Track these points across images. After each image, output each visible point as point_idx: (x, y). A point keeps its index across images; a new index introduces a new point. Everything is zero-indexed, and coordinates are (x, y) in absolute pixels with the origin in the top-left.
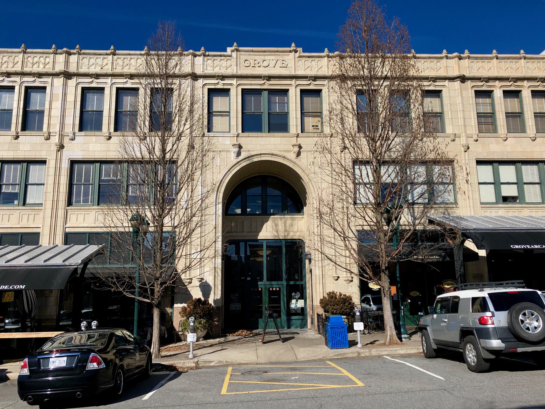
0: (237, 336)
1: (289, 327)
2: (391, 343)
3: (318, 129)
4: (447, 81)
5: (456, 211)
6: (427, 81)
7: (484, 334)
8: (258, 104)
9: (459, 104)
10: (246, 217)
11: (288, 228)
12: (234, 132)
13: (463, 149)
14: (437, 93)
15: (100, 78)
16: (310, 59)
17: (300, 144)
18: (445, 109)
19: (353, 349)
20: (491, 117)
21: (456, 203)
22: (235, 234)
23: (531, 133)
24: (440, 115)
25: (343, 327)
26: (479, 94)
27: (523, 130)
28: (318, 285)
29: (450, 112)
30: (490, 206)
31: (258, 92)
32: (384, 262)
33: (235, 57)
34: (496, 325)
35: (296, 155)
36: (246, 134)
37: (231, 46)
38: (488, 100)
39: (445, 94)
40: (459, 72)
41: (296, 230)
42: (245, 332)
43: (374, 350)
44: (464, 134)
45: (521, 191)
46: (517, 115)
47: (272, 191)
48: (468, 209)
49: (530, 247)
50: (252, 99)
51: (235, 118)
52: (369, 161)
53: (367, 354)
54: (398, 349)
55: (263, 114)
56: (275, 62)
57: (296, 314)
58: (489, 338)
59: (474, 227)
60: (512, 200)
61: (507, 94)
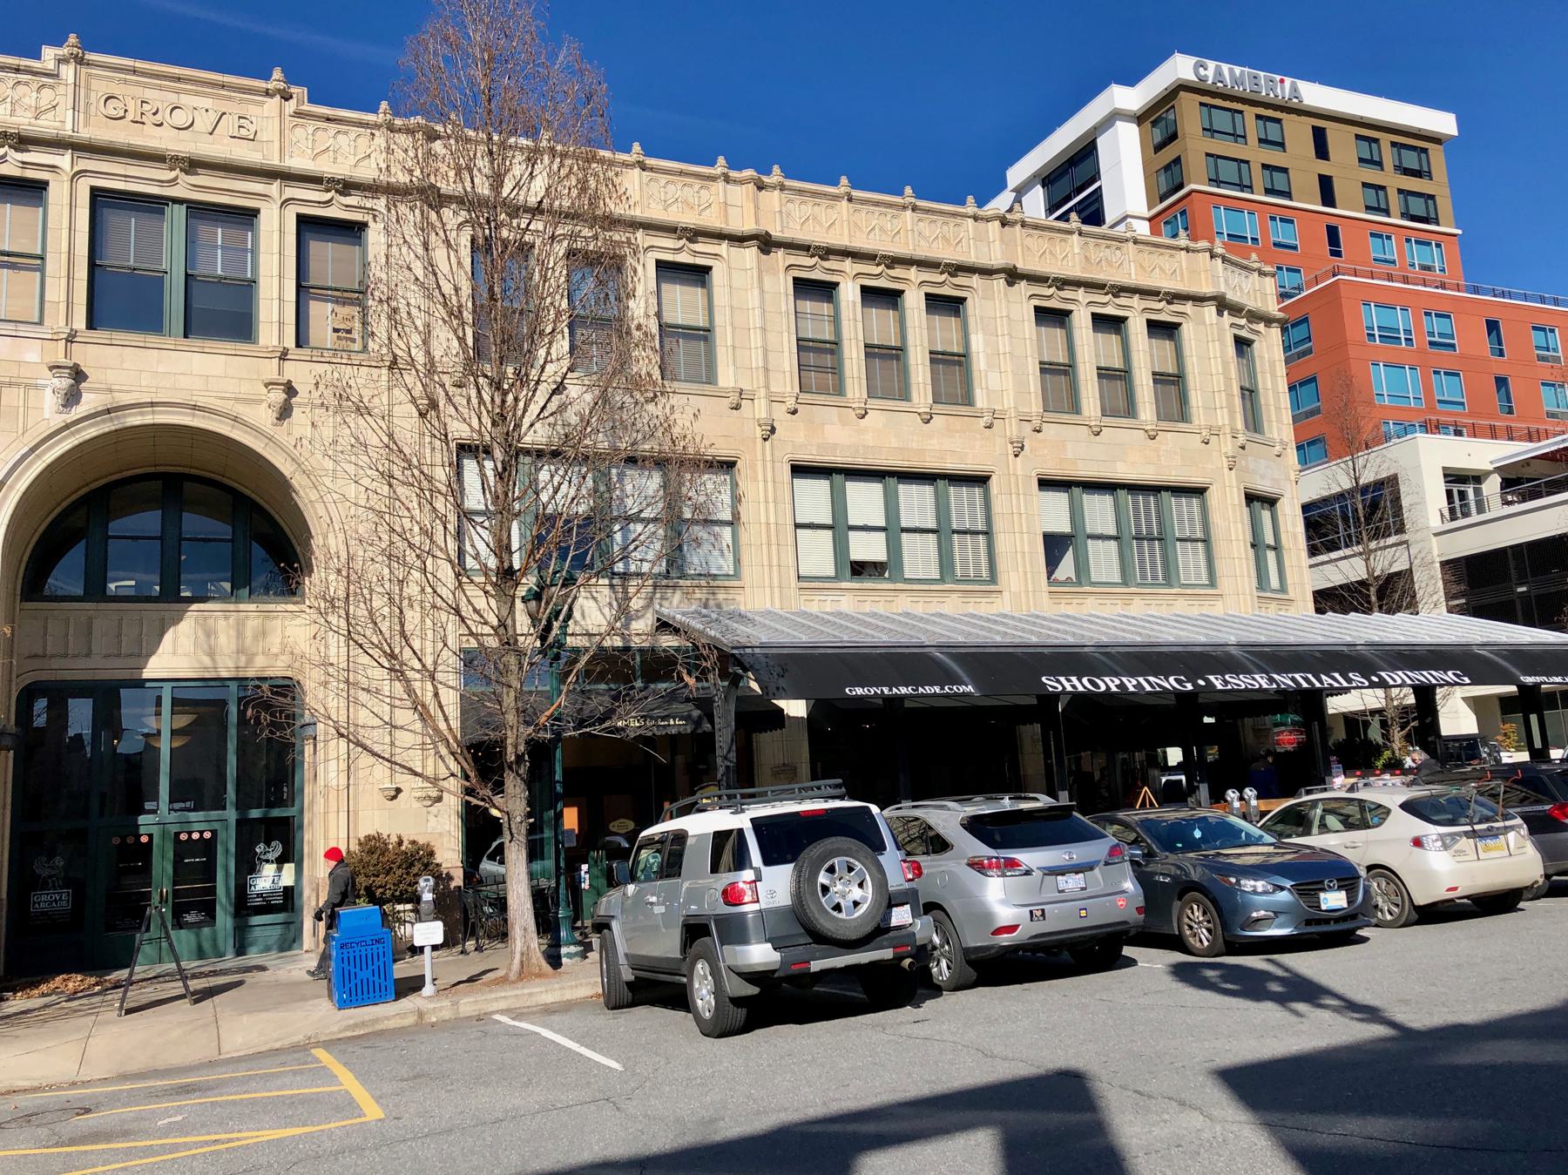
0: (43, 995)
1: (241, 950)
2: (524, 974)
3: (354, 341)
4: (725, 244)
5: (737, 597)
6: (674, 236)
7: (734, 931)
8: (153, 244)
9: (753, 309)
10: (103, 606)
11: (248, 641)
12: (56, 321)
13: (759, 433)
14: (698, 274)
15: (31, 147)
16: (333, 127)
17: (289, 382)
18: (718, 320)
19: (409, 1003)
20: (832, 352)
21: (737, 575)
22: (56, 664)
23: (922, 401)
24: (704, 335)
25: (378, 941)
26: (804, 287)
27: (905, 395)
28: (332, 816)
29: (729, 329)
30: (821, 585)
31: (153, 205)
32: (515, 740)
33: (71, 80)
34: (764, 904)
35: (275, 415)
36: (99, 335)
37: (59, 42)
38: (826, 308)
39: (717, 276)
40: (757, 222)
41: (275, 650)
42: (75, 981)
43: (465, 1000)
44: (762, 392)
45: (894, 548)
46: (826, 349)
47: (193, 523)
48: (768, 590)
49: (891, 690)
50: (129, 225)
51: (64, 281)
52: (470, 446)
53: (446, 1014)
54: (538, 990)
55: (167, 278)
56: (213, 117)
57: (267, 908)
58: (744, 941)
59: (764, 639)
60: (872, 570)
61: (873, 295)
